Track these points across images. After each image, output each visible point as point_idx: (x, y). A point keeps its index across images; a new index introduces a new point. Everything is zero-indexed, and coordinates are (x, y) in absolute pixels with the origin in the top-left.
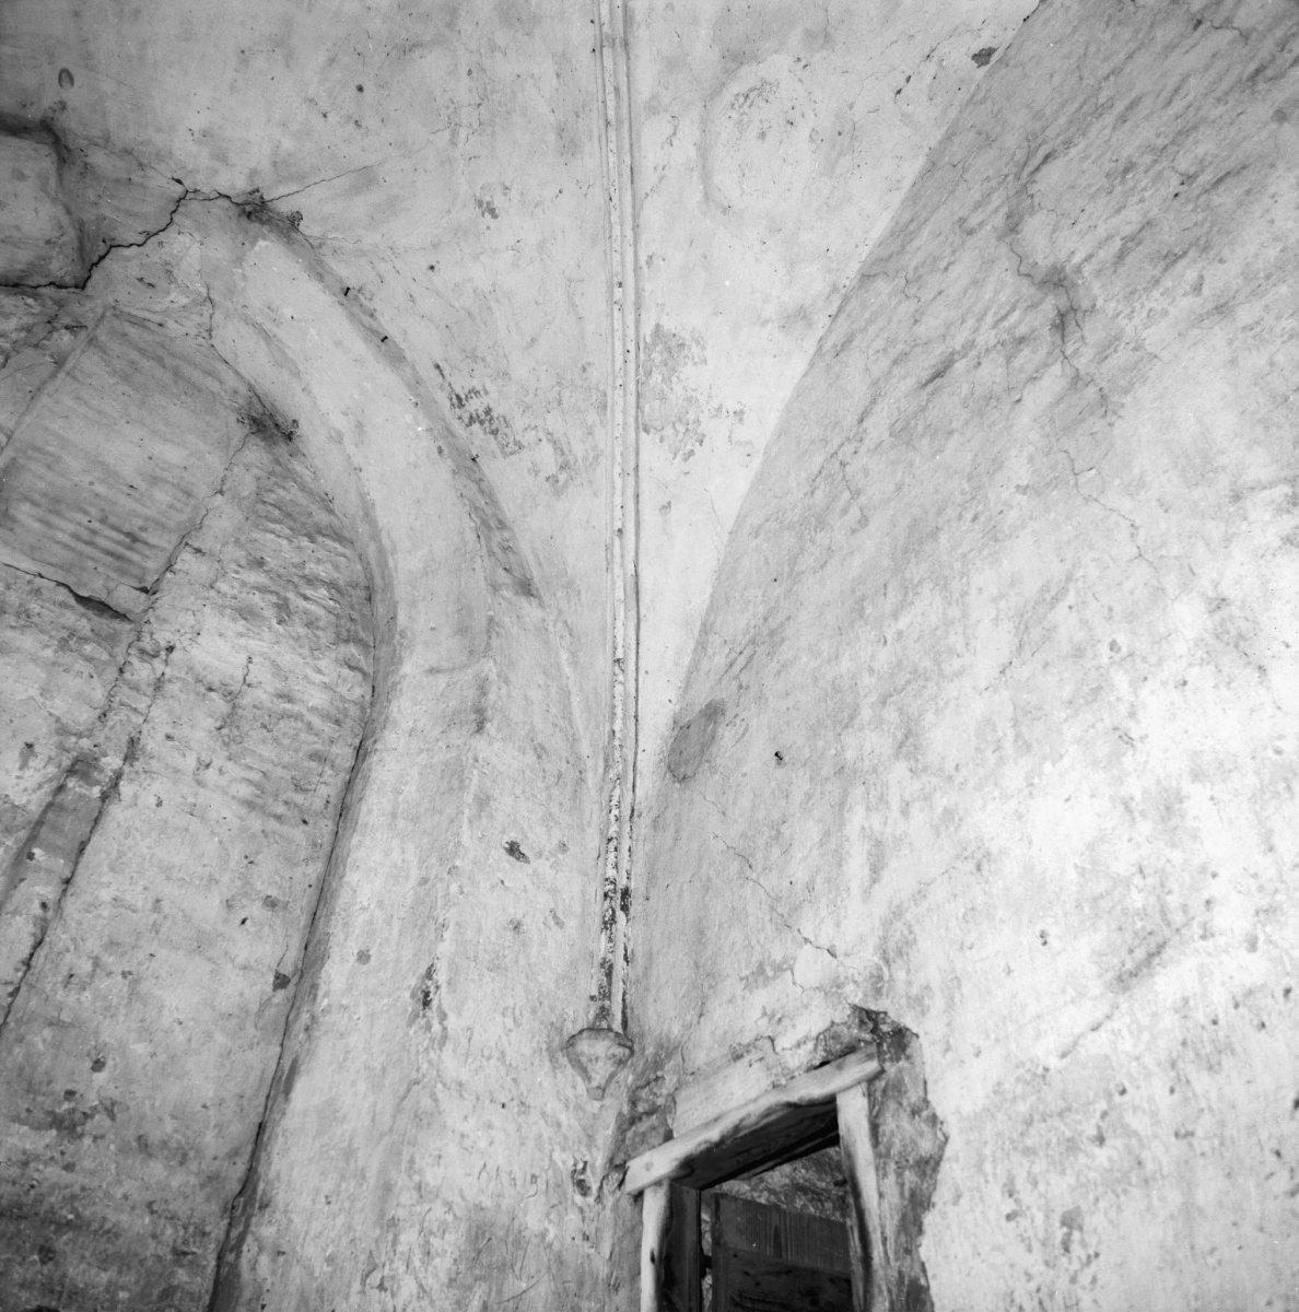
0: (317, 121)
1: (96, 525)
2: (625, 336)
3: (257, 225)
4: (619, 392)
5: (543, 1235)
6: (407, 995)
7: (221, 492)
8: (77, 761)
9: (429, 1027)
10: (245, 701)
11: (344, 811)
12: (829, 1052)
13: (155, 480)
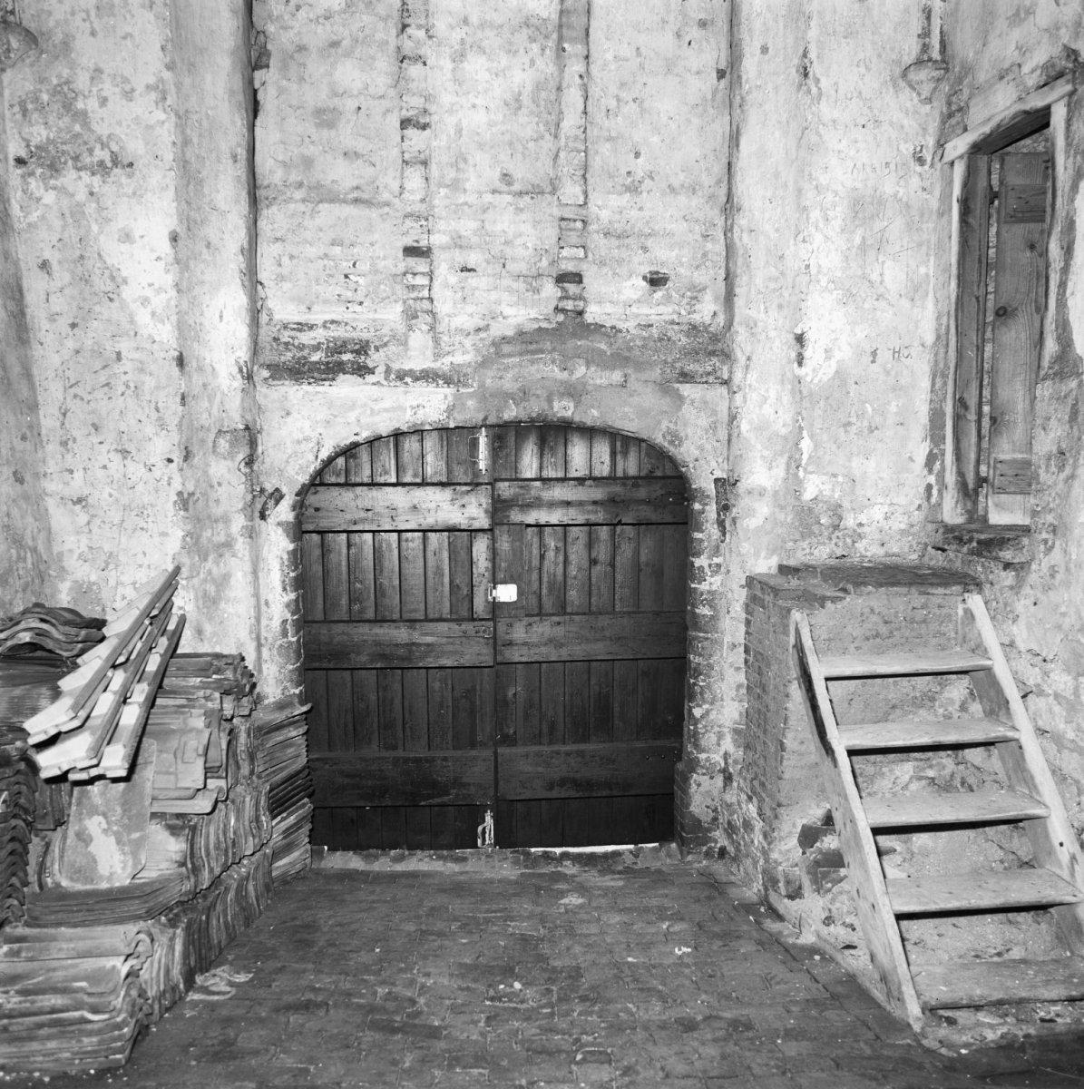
9: (809, 91)
12: (1048, 76)
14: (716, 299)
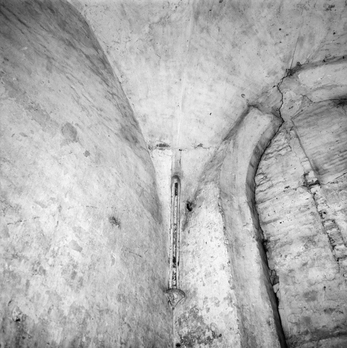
1: (341, 154)
3: (294, 74)
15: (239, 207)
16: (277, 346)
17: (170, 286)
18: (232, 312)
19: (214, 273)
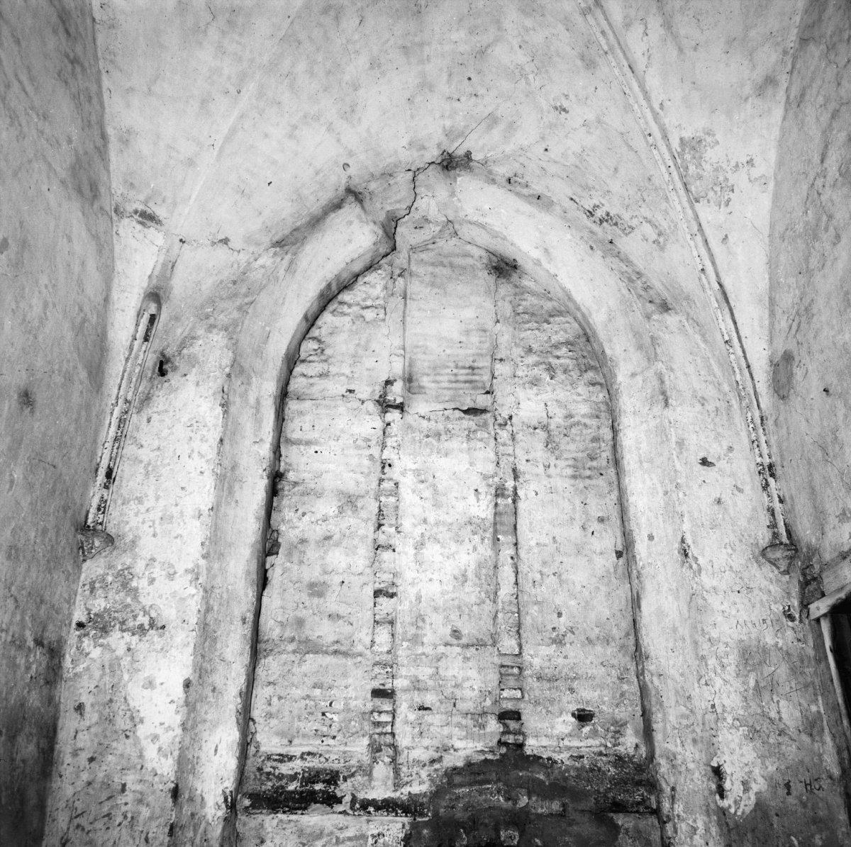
0: (457, 104)
1: (455, 371)
2: (664, 160)
4: (674, 193)
5: (776, 644)
6: (676, 552)
7: (498, 321)
8: (497, 490)
10: (552, 427)
11: (617, 462)
13: (467, 332)
14: (636, 733)
15: (258, 402)
16: (246, 655)
17: (90, 521)
18: (193, 596)
19: (179, 520)
